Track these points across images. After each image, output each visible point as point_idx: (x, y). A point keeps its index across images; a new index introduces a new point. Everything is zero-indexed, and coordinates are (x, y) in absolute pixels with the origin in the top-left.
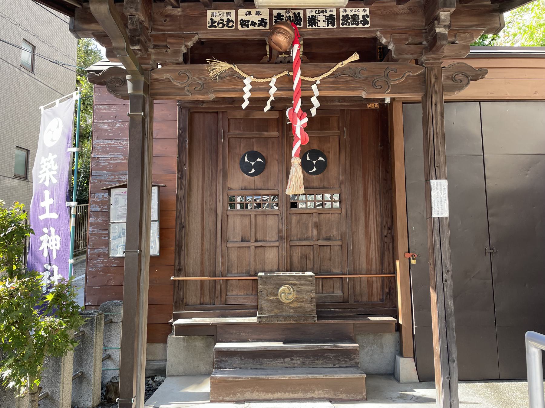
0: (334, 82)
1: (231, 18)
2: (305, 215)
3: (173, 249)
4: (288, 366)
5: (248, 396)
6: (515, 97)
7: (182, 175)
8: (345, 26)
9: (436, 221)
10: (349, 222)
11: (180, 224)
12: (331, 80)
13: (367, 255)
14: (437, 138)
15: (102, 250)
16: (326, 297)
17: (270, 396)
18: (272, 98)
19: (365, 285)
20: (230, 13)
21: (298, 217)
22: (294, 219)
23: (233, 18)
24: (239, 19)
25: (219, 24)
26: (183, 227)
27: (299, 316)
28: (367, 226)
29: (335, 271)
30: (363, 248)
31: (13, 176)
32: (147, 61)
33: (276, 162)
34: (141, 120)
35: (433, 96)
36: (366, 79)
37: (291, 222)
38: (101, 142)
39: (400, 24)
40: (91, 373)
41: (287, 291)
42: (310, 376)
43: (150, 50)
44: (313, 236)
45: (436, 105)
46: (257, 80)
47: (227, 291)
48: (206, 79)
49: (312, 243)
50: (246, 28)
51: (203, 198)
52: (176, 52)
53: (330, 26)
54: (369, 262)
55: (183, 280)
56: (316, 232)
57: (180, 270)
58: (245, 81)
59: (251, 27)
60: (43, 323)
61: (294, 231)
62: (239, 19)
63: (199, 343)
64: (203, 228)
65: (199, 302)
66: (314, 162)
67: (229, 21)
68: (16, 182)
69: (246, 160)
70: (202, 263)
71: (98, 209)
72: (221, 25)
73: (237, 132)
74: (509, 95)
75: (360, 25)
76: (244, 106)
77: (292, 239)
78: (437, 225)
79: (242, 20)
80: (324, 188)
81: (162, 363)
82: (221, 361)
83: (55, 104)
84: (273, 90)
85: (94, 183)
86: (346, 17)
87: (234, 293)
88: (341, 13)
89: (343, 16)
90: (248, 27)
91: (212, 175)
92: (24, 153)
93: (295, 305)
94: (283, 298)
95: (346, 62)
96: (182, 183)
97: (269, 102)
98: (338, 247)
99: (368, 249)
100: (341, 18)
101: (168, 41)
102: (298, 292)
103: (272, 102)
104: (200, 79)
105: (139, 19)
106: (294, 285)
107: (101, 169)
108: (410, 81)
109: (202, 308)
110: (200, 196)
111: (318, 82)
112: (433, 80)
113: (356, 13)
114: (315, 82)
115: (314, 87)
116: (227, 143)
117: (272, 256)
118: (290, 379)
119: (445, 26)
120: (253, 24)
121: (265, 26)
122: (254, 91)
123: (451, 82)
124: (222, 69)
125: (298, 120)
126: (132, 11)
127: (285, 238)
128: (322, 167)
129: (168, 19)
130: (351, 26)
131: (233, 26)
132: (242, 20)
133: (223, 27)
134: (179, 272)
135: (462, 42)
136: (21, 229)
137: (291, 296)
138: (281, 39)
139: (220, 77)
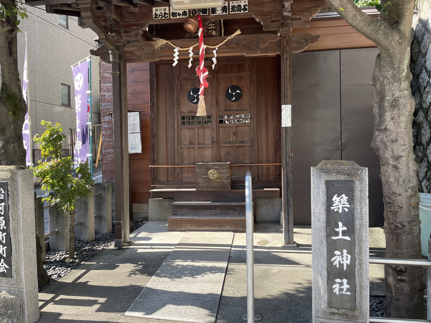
0: (226, 48)
1: (166, 12)
2: (228, 128)
3: (150, 149)
4: (213, 214)
5: (188, 228)
6: (365, 45)
7: (153, 104)
8: (233, 13)
9: (284, 129)
10: (256, 131)
11: (153, 134)
12: (225, 47)
13: (267, 152)
14: (287, 79)
15: (110, 150)
16: (240, 177)
17: (201, 228)
18: (191, 59)
19: (265, 170)
20: (165, 9)
21: (224, 129)
22: (221, 130)
23: (167, 12)
24: (171, 12)
25: (159, 16)
26: (155, 136)
27: (220, 187)
28: (267, 133)
29: (246, 161)
30: (264, 148)
31: (60, 105)
32: (121, 41)
33: (210, 94)
34: (118, 76)
35: (285, 54)
36: (245, 45)
37: (219, 133)
38: (105, 85)
39: (266, 9)
40: (106, 215)
41: (213, 173)
42: (222, 218)
43: (122, 34)
44: (233, 141)
45: (286, 59)
46: (181, 49)
47: (182, 174)
48: (153, 50)
49: (232, 145)
50: (175, 18)
51: (166, 118)
52: (137, 35)
53: (224, 13)
54: (268, 156)
55: (156, 167)
56: (234, 138)
57: (154, 161)
58: (175, 50)
59: (178, 17)
60: (74, 181)
61: (221, 138)
62: (171, 12)
63: (166, 203)
64: (166, 137)
65: (166, 180)
66: (234, 94)
67: (165, 14)
68: (62, 108)
69: (191, 94)
70: (167, 157)
71: (107, 126)
72: (161, 17)
73: (186, 76)
74: (360, 43)
75: (242, 12)
76: (174, 65)
77: (220, 142)
78: (284, 131)
79: (173, 12)
80: (240, 110)
81: (147, 214)
82: (175, 211)
83: (78, 64)
84: (192, 54)
85: (103, 110)
86: (233, 7)
87: (186, 175)
88: (231, 5)
89: (232, 6)
90: (176, 17)
91: (171, 104)
92: (67, 88)
93: (218, 181)
94: (211, 176)
95: (233, 36)
96: (153, 109)
97: (190, 62)
98: (248, 147)
99: (267, 148)
100: (231, 7)
101: (132, 28)
102: (219, 173)
103: (192, 62)
104: (150, 50)
105: (113, 18)
106: (217, 169)
107: (106, 102)
108: (272, 45)
109: (167, 184)
110: (164, 117)
111: (217, 49)
112: (285, 44)
113: (240, 4)
114: (215, 49)
115: (215, 52)
116: (179, 83)
117: (208, 153)
118: (211, 220)
119: (288, 11)
120: (179, 14)
121: (186, 16)
122: (181, 55)
123: (296, 45)
124: (162, 44)
125: (202, 73)
126: (109, 14)
127: (216, 142)
128: (239, 97)
129: (131, 15)
130: (236, 12)
131: (167, 17)
132: (173, 12)
133: (162, 17)
134: (154, 163)
135: (304, 19)
136: (60, 136)
137: (215, 176)
138: (190, 27)
139: (161, 48)
